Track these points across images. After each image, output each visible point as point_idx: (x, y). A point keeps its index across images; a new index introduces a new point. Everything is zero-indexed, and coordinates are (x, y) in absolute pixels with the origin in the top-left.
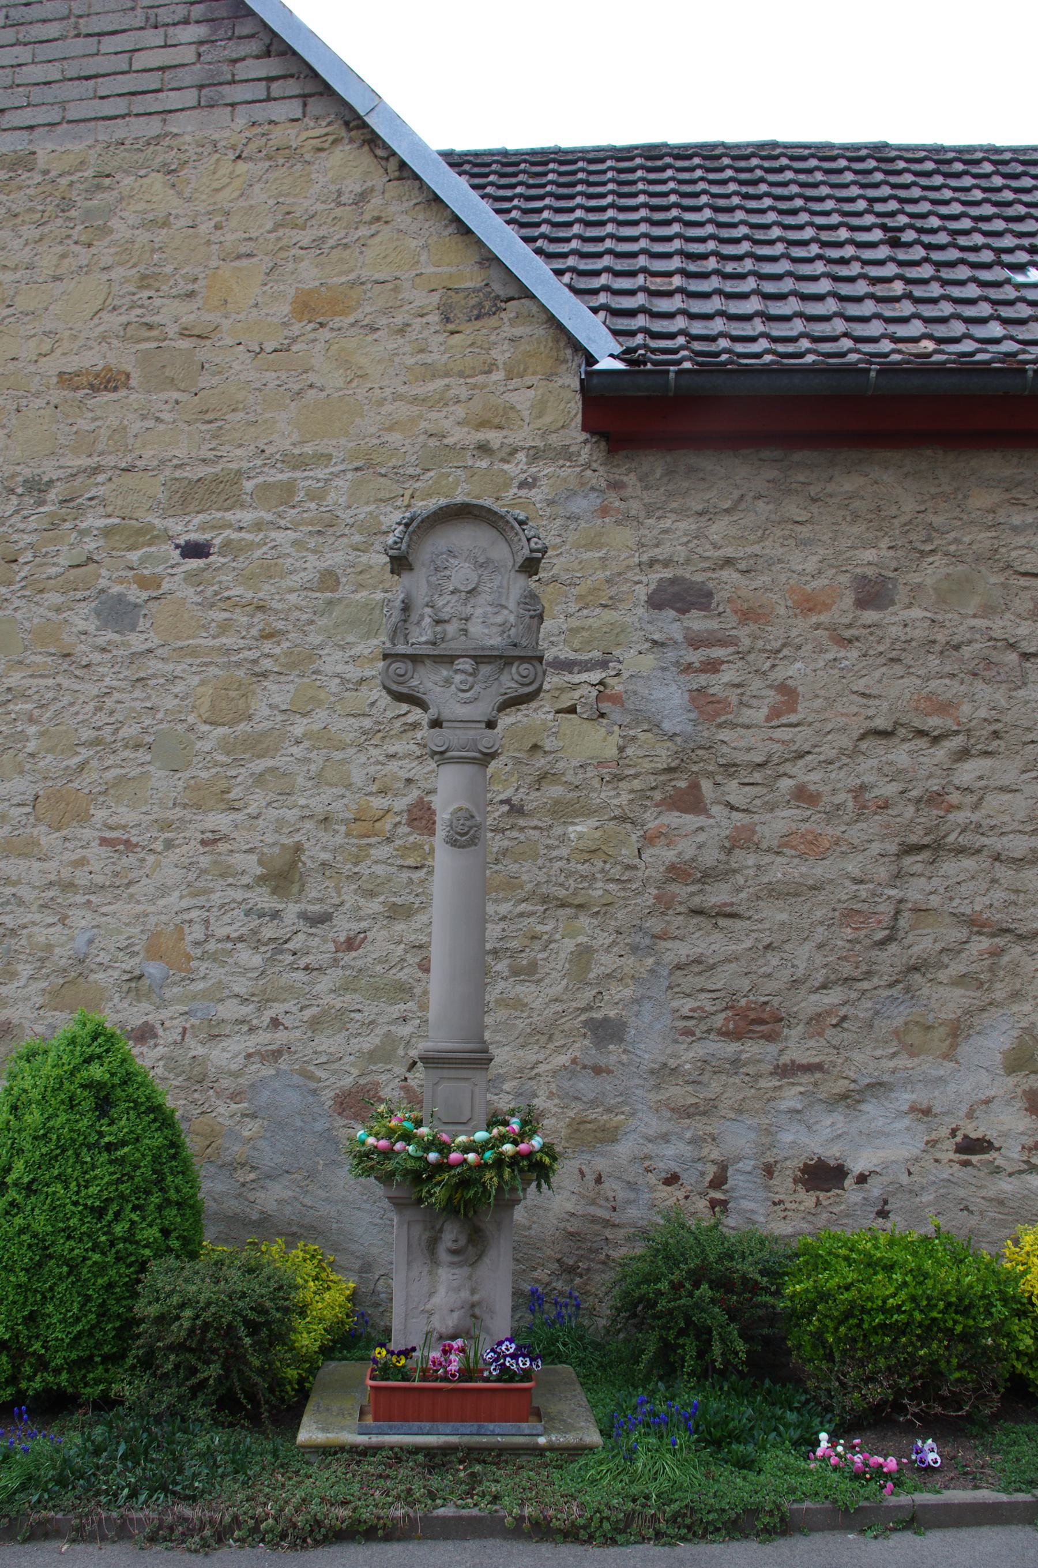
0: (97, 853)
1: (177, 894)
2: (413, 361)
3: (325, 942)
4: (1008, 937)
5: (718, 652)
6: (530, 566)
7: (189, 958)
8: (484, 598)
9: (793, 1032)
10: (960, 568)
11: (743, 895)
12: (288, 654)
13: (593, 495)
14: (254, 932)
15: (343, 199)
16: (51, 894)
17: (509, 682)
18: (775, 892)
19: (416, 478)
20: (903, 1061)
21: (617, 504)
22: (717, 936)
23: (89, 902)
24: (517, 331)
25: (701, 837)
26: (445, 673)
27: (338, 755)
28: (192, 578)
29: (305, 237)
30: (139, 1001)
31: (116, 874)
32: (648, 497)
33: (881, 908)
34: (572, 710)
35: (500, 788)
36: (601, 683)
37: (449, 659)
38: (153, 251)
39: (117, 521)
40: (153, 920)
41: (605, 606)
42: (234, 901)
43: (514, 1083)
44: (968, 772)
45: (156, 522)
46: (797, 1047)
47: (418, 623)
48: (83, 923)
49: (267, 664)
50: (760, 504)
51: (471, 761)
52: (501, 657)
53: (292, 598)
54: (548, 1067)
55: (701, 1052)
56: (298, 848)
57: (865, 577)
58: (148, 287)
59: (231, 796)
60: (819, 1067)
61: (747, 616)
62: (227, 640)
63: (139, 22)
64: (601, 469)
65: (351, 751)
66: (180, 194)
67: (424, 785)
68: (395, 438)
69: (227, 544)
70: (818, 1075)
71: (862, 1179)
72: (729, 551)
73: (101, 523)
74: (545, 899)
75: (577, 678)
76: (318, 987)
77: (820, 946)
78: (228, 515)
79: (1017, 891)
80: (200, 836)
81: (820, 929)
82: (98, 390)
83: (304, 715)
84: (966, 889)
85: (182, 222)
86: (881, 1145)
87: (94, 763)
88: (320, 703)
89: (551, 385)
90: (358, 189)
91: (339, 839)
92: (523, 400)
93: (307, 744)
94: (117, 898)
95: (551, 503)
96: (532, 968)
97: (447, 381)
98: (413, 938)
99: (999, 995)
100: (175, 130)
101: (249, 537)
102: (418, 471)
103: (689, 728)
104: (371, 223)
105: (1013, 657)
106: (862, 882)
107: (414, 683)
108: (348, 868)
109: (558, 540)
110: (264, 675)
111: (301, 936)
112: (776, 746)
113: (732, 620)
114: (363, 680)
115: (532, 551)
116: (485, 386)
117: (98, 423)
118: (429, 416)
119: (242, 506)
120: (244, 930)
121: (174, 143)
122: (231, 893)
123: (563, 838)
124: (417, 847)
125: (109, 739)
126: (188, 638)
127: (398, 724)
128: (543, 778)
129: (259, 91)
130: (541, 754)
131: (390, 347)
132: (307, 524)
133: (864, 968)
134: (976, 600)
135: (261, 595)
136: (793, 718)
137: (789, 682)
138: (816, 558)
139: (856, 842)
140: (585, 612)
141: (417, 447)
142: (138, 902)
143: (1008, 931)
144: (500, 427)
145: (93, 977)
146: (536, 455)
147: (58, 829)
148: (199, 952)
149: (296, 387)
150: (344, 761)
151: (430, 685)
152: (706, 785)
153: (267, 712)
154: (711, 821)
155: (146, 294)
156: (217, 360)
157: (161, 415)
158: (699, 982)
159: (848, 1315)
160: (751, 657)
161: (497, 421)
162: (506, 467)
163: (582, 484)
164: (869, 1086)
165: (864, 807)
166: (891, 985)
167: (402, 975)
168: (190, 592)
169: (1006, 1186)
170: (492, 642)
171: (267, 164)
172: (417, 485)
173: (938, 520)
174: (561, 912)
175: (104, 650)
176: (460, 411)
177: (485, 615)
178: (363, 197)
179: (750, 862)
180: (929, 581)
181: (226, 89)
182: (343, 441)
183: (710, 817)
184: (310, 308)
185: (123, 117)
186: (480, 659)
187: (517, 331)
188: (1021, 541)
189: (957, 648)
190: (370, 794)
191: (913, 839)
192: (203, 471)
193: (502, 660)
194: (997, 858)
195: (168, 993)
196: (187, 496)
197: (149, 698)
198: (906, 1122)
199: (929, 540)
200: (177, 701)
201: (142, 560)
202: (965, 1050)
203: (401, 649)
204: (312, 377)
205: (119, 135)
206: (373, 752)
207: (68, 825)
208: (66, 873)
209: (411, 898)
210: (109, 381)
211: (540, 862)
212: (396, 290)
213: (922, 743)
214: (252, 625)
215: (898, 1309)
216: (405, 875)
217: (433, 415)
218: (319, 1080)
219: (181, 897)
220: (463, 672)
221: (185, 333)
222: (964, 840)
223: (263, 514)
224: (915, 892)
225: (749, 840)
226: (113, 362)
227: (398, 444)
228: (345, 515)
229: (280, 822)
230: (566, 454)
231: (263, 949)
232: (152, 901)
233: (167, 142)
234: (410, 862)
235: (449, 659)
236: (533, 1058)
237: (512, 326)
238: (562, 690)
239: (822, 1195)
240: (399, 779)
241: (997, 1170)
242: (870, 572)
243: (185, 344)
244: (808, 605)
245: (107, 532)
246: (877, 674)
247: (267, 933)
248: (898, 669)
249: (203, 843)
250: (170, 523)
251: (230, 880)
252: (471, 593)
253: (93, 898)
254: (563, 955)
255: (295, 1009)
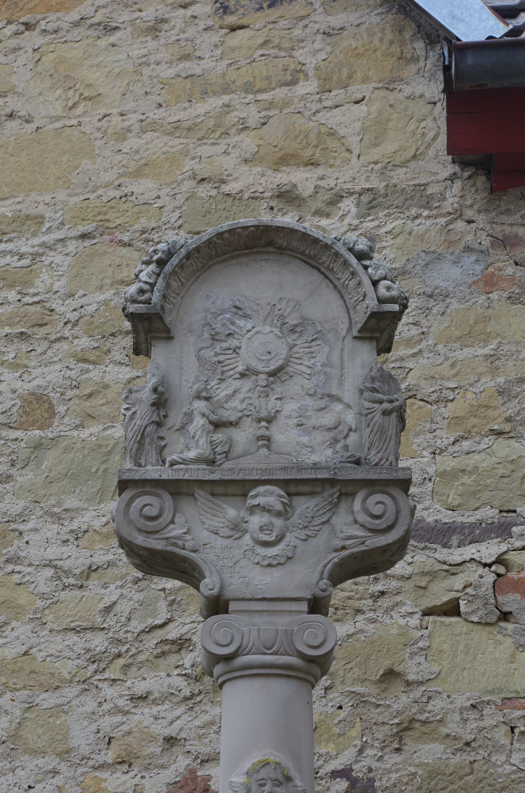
2: (172, 72)
6: (379, 329)
8: (296, 386)
13: (469, 260)
17: (350, 527)
21: (510, 270)
24: (336, 20)
26: (232, 513)
27: (47, 700)
34: (452, 609)
35: (331, 749)
36: (500, 560)
37: (238, 489)
41: (499, 433)
47: (183, 428)
51: (284, 672)
52: (332, 482)
67: (195, 746)
68: (144, 187)
75: (457, 555)
88: (18, 611)
89: (392, 96)
92: (348, 121)
97: (226, 98)
107: (176, 531)
109: (415, 331)
114: (91, 570)
115: (381, 301)
116: (286, 104)
118: (199, 151)
127: (151, 641)
128: (405, 730)
130: (399, 687)
131: (135, 53)
140: (466, 445)
141: (180, 199)
144: (312, 163)
146: (371, 202)
150: (60, 709)
151: (204, 535)
161: (307, 153)
170: (315, 458)
176: (248, 143)
177: (302, 413)
182: (61, 196)
186: (295, 487)
190: (102, 767)
193: (334, 488)
203: (152, 471)
206: (108, 691)
217: (206, 150)
220: (265, 509)
227: (148, 196)
228: (65, 309)
230: (421, 197)
235: (238, 489)
237: (326, 12)
238: (432, 575)
240: (153, 738)
252: (278, 376)
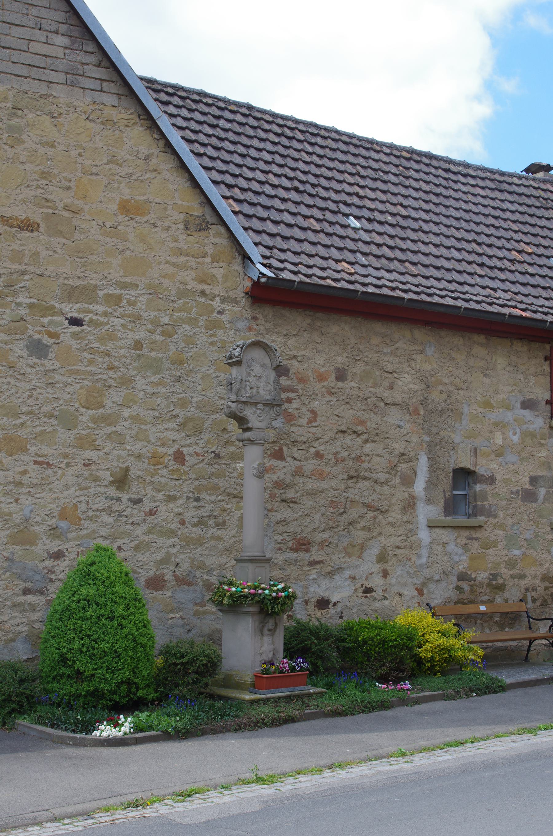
0: (31, 467)
1: (73, 489)
3: (140, 511)
4: (379, 512)
5: (292, 395)
7: (80, 519)
8: (263, 379)
9: (313, 549)
10: (368, 367)
11: (298, 494)
12: (121, 378)
14: (109, 507)
15: (140, 156)
16: (10, 487)
18: (310, 494)
19: (174, 302)
20: (347, 559)
21: (255, 326)
22: (289, 510)
23: (29, 492)
25: (285, 471)
27: (144, 427)
28: (74, 335)
29: (123, 171)
30: (54, 540)
31: (43, 479)
32: (268, 325)
33: (342, 500)
35: (210, 446)
38: (48, 159)
39: (36, 301)
40: (63, 501)
42: (100, 493)
43: (218, 571)
44: (368, 448)
45: (56, 304)
46: (316, 555)
48: (27, 502)
49: (111, 382)
50: (305, 333)
53: (122, 351)
54: (230, 564)
55: (285, 557)
56: (127, 469)
57: (339, 368)
58: (45, 178)
59: (97, 443)
60: (319, 562)
61: (302, 380)
62: (92, 368)
63: (31, 24)
64: (249, 310)
65: (149, 426)
66: (59, 131)
68: (166, 281)
69: (91, 321)
70: (322, 565)
71: (335, 604)
72: (295, 352)
73: (28, 301)
74: (229, 494)
76: (137, 532)
77: (323, 515)
78: (91, 307)
79: (381, 495)
80: (83, 462)
81: (323, 508)
82: (23, 230)
83: (128, 407)
84: (366, 493)
85: (61, 147)
86: (340, 591)
87: (29, 423)
88: (135, 402)
90: (147, 153)
91: (145, 466)
93: (130, 421)
94: (44, 490)
95: (230, 322)
96: (224, 523)
97: (187, 258)
98: (177, 510)
99: (375, 534)
100: (55, 94)
101: (101, 319)
102: (176, 299)
103: (281, 426)
104: (152, 171)
105: (382, 404)
106: (336, 490)
108: (148, 479)
110: (109, 387)
111: (130, 509)
112: (310, 435)
113: (296, 382)
117: (23, 247)
119: (97, 303)
120: (105, 506)
121: (55, 101)
122: (99, 489)
123: (235, 469)
124: (178, 470)
125: (37, 412)
126: (73, 365)
127: (169, 415)
129: (96, 85)
131: (163, 236)
132: (128, 317)
133: (336, 523)
134: (372, 381)
135: (107, 348)
136: (315, 424)
137: (315, 409)
138: (323, 359)
139: (335, 474)
142: (54, 492)
143: (379, 509)
145: (32, 528)
146: (224, 300)
147: (11, 455)
148: (84, 516)
149: (121, 248)
150: (146, 430)
152: (285, 449)
153: (111, 405)
154: (287, 464)
155: (45, 182)
156: (83, 226)
157: (57, 250)
158: (284, 529)
159: (379, 644)
160: (302, 398)
162: (212, 303)
163: (242, 316)
164: (338, 568)
165: (337, 461)
166: (343, 530)
167: (173, 526)
168: (74, 342)
169: (378, 605)
171: (102, 127)
172: (175, 305)
173: (362, 347)
174: (234, 500)
175: (32, 367)
178: (148, 157)
179: (301, 481)
180: (358, 372)
181: (81, 79)
182: (143, 279)
183: (287, 462)
184: (125, 208)
185: (26, 77)
187: (217, 240)
188: (386, 358)
189: (366, 399)
190: (157, 446)
191: (352, 474)
192: (78, 283)
194: (376, 482)
195: (70, 536)
196: (71, 294)
197: (55, 393)
198: (348, 582)
199: (358, 355)
200: (69, 396)
201: (51, 323)
202: (365, 554)
204: (129, 245)
205: (25, 87)
206: (158, 427)
207: (16, 454)
208: (18, 478)
209: (176, 493)
210: (28, 226)
211: (226, 479)
212: (165, 209)
213: (354, 436)
214: (103, 363)
215: (395, 640)
216: (173, 482)
218: (139, 573)
219: (76, 491)
221: (66, 208)
222: (367, 474)
223: (107, 308)
224: (351, 494)
225: (300, 472)
226: (30, 217)
228: (144, 315)
229: (119, 457)
230: (235, 301)
231: (113, 515)
232: (61, 492)
233: (51, 99)
234: (175, 477)
236: (225, 561)
239: (323, 611)
240: (170, 440)
241: (375, 599)
242: (340, 366)
243: (66, 214)
244: (321, 378)
245: (31, 306)
246: (342, 408)
247: (115, 507)
248: (348, 406)
249: (84, 465)
250: (63, 306)
251: (98, 483)
253: (31, 490)
254: (235, 518)
255: (127, 542)
